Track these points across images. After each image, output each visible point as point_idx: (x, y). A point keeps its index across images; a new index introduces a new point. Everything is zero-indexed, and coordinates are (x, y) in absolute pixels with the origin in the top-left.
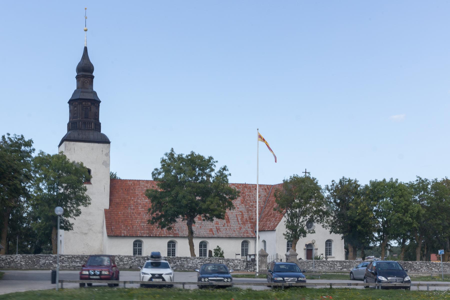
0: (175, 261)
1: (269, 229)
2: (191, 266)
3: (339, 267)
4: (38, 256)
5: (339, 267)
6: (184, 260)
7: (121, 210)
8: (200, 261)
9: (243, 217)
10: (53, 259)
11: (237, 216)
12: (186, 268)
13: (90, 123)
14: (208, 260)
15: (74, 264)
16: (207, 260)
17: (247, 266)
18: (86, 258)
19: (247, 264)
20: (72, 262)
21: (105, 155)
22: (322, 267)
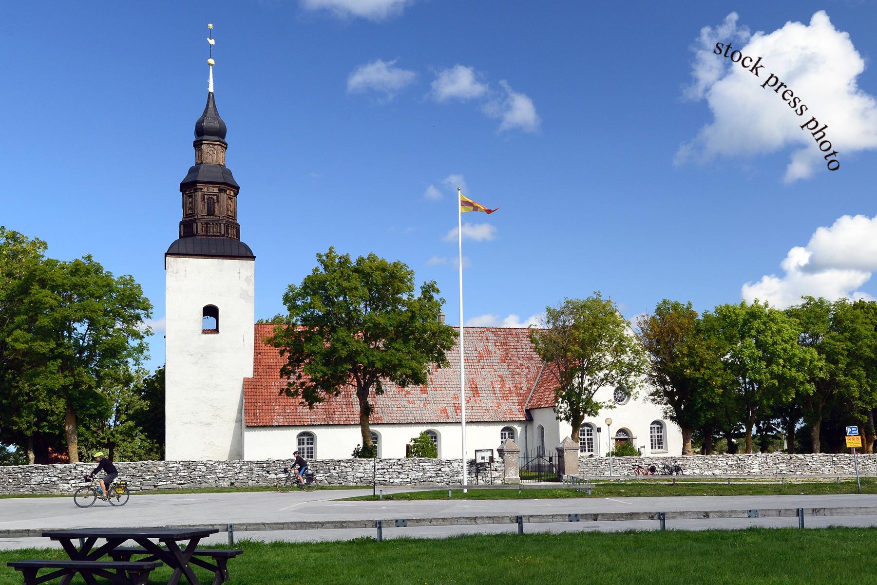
0: (327, 467)
9: (503, 386)
21: (245, 280)
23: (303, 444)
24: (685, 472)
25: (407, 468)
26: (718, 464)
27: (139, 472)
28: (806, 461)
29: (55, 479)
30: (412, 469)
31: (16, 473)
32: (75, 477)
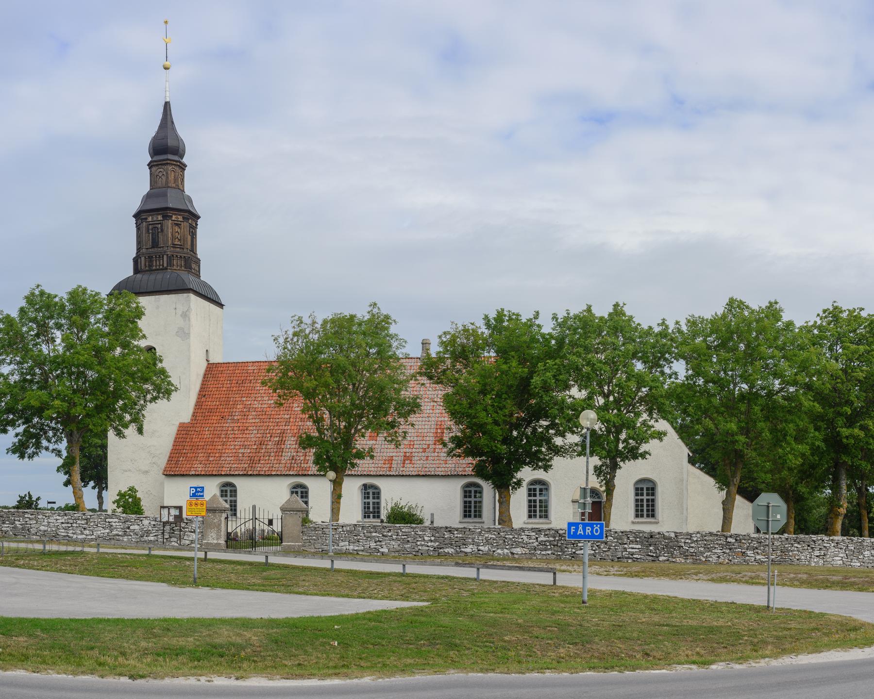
0: (13, 518)
3: (429, 544)
5: (429, 544)
8: (63, 521)
16: (78, 519)
21: (181, 316)
24: (464, 548)
25: (92, 524)
26: (520, 540)
28: (677, 541)
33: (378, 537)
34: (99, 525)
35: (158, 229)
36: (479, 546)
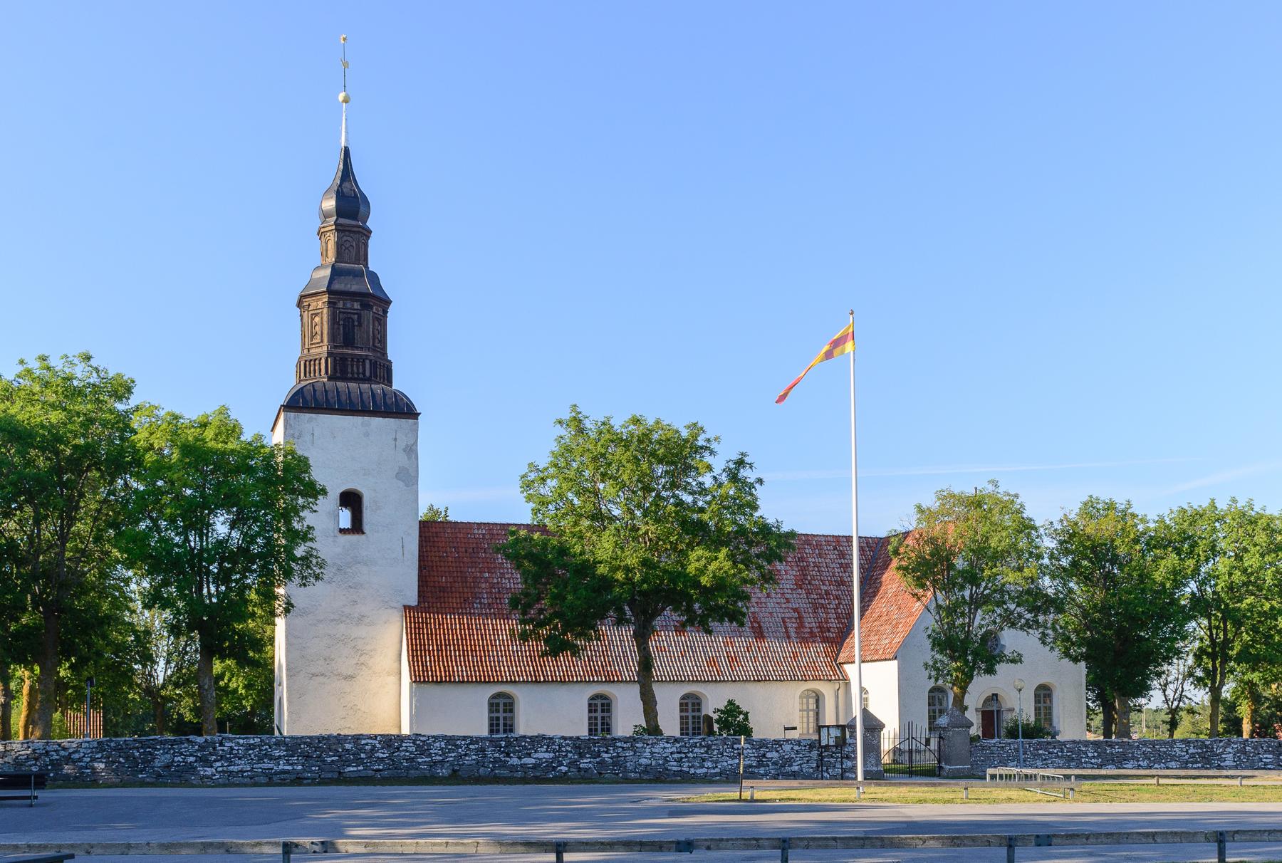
0: (596, 749)
1: (876, 658)
2: (646, 766)
3: (1093, 761)
4: (147, 740)
5: (1093, 761)
6: (625, 745)
7: (453, 608)
8: (674, 749)
9: (801, 625)
10: (198, 750)
11: (784, 622)
12: (632, 772)
13: (358, 361)
14: (701, 744)
15: (268, 764)
17: (822, 760)
18: (309, 745)
19: (820, 755)
20: (260, 759)
22: (1045, 759)
23: (498, 711)
26: (1174, 753)
27: (316, 751)
29: (192, 759)
30: (722, 754)
31: (130, 749)
32: (222, 756)
33: (1044, 754)
34: (725, 754)
35: (353, 321)
36: (1139, 761)
